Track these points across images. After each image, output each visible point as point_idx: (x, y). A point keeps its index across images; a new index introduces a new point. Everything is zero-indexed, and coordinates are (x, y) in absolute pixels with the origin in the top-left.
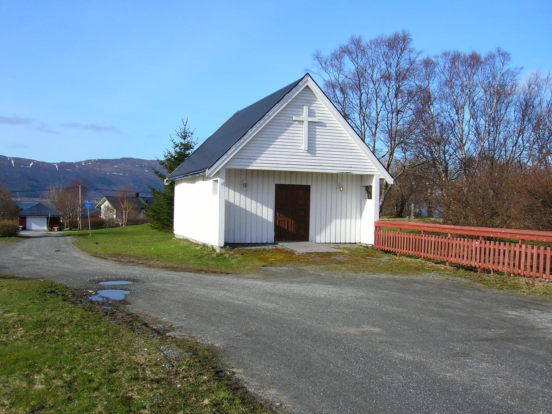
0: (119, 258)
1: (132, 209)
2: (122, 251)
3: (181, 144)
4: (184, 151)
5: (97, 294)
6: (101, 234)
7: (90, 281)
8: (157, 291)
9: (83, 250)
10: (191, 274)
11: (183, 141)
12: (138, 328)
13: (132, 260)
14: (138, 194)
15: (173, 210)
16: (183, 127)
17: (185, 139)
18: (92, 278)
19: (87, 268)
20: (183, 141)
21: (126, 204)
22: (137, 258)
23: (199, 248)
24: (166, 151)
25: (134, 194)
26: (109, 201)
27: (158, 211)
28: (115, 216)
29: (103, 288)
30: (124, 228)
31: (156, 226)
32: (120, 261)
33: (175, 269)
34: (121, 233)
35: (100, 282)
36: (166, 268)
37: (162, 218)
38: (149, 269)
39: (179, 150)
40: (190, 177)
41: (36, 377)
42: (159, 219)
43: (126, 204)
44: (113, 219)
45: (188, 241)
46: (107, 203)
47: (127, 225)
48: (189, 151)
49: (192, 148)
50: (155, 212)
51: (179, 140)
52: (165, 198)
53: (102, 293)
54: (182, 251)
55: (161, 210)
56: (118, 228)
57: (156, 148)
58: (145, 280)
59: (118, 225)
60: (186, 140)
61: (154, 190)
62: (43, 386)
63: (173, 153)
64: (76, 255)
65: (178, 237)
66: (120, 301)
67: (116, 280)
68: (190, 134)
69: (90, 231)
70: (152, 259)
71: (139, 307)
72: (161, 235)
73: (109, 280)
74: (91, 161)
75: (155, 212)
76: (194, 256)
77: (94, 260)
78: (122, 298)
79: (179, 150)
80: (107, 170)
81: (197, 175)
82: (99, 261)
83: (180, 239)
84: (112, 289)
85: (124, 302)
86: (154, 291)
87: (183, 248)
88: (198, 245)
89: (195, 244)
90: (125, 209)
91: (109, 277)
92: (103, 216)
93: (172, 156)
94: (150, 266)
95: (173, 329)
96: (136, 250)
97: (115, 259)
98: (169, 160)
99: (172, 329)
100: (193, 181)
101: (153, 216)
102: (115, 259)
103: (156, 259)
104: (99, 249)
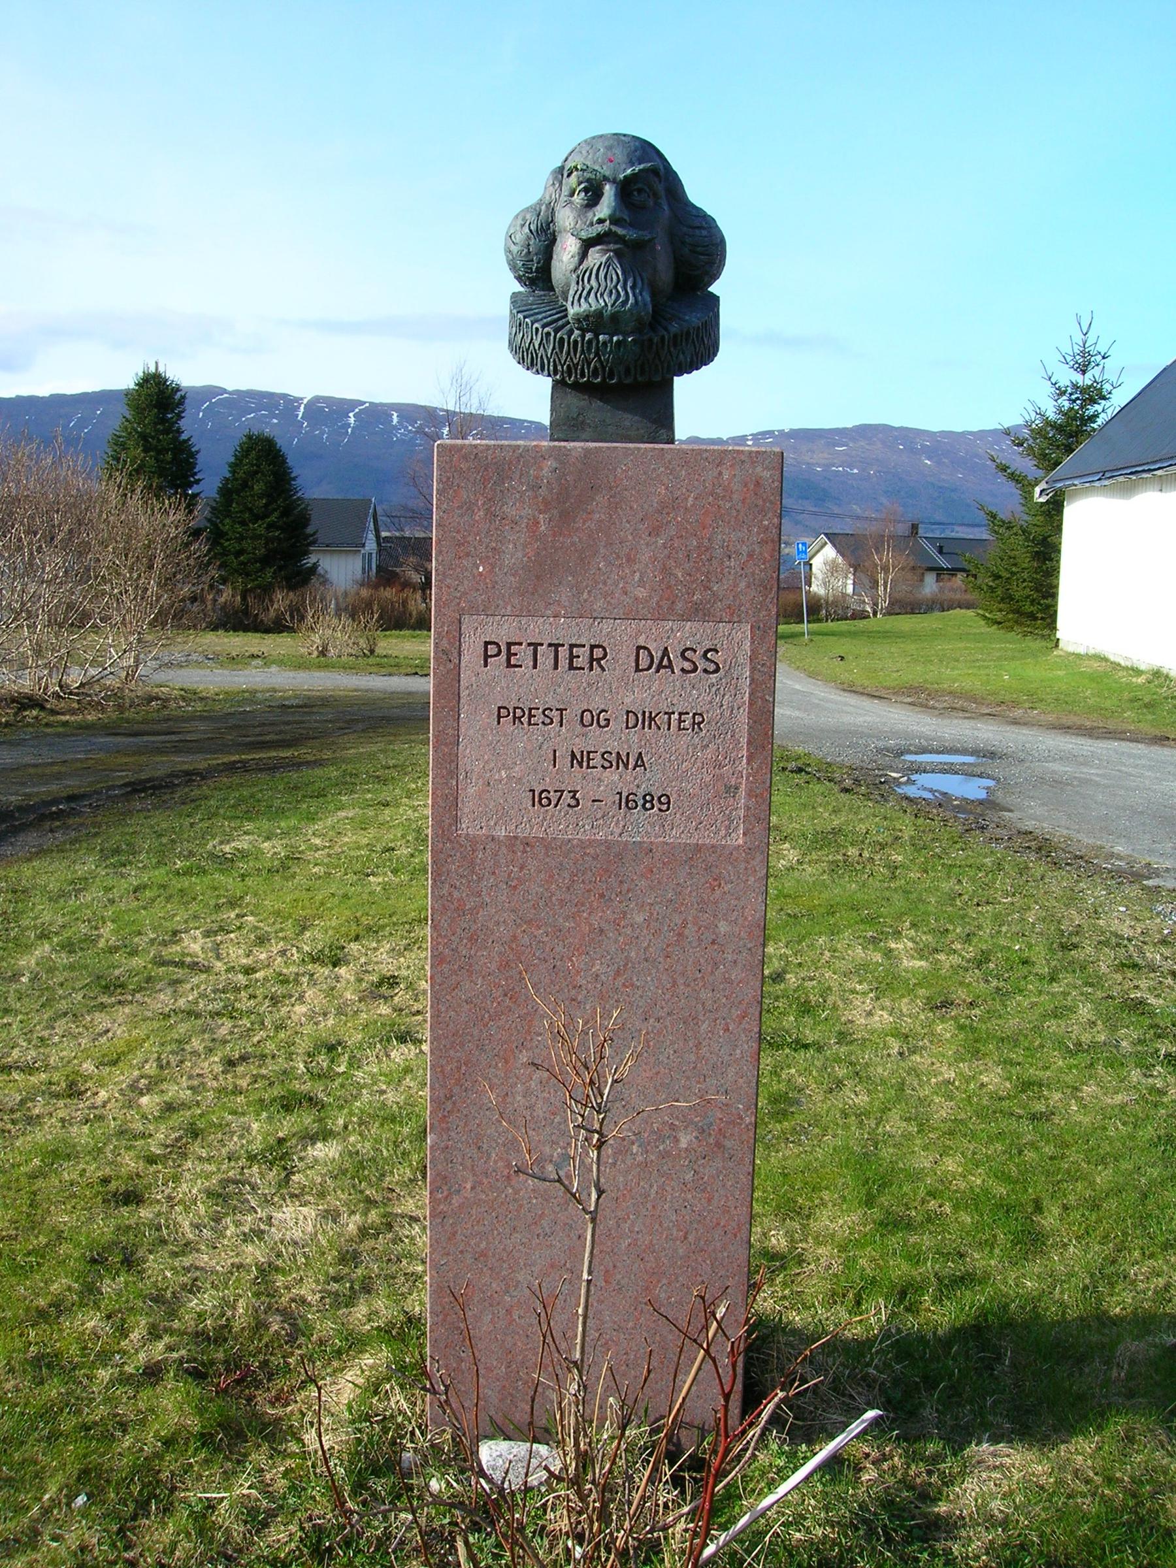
0: (920, 696)
1: (903, 569)
2: (926, 681)
3: (1075, 386)
4: (1082, 407)
5: (910, 782)
6: (833, 634)
7: (879, 751)
8: (1068, 784)
9: (813, 675)
10: (1140, 746)
11: (1078, 378)
12: (1068, 864)
13: (960, 703)
14: (915, 527)
15: (1054, 572)
16: (1079, 338)
17: (1084, 372)
18: (881, 744)
19: (847, 719)
20: (1078, 378)
21: (888, 556)
22: (974, 699)
23: (1141, 680)
24: (1030, 408)
25: (903, 529)
26: (834, 545)
27: (1006, 575)
28: (850, 589)
29: (921, 769)
30: (880, 622)
31: (999, 616)
32: (926, 707)
33: (1089, 732)
34: (869, 635)
35: (902, 754)
36: (1066, 729)
37: (1017, 596)
38: (1014, 728)
39: (1067, 404)
40: (1121, 479)
41: (893, 946)
42: (1008, 598)
43: (888, 556)
44: (844, 595)
45: (1106, 660)
46: (829, 552)
47: (890, 614)
48: (1097, 407)
49: (1104, 398)
50: (997, 577)
51: (1067, 377)
52: (1027, 540)
53: (922, 779)
54: (1094, 685)
55: (1013, 574)
56: (865, 622)
57: (1004, 396)
58: (1022, 755)
59: (863, 616)
60: (1089, 375)
61: (994, 516)
62: (923, 963)
63: (1051, 414)
64: (797, 687)
65: (1071, 649)
66: (981, 802)
67: (942, 752)
68: (1099, 358)
69: (805, 627)
70: (1015, 704)
71: (1033, 814)
72: (1010, 642)
73: (924, 751)
74: (770, 433)
75: (997, 577)
76: (1131, 701)
77: (853, 700)
78: (982, 795)
79: (1067, 404)
80: (817, 460)
81: (1145, 475)
82: (866, 703)
83: (1078, 656)
84: (944, 771)
85: (989, 804)
86: (1058, 783)
87: (1094, 678)
88: (1138, 672)
89: (1126, 668)
90: (885, 569)
91: (924, 743)
92: (817, 588)
93: (1047, 422)
94: (1015, 722)
95: (1157, 874)
96: (959, 677)
97: (909, 700)
98: (1039, 433)
99: (1157, 874)
100: (1127, 490)
101: (992, 589)
102: (909, 700)
103: (1027, 705)
104: (854, 672)
